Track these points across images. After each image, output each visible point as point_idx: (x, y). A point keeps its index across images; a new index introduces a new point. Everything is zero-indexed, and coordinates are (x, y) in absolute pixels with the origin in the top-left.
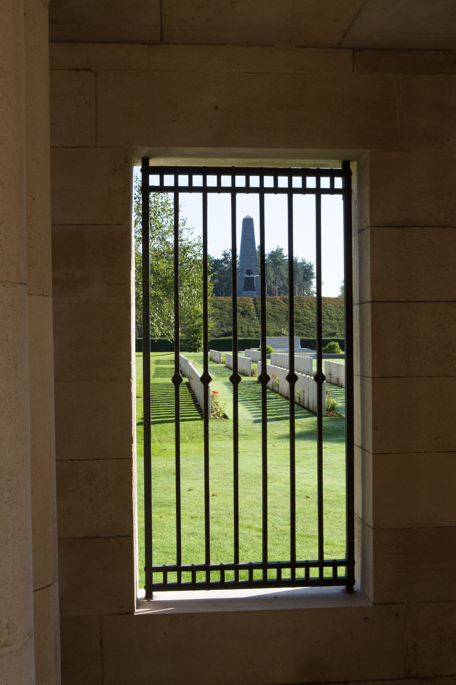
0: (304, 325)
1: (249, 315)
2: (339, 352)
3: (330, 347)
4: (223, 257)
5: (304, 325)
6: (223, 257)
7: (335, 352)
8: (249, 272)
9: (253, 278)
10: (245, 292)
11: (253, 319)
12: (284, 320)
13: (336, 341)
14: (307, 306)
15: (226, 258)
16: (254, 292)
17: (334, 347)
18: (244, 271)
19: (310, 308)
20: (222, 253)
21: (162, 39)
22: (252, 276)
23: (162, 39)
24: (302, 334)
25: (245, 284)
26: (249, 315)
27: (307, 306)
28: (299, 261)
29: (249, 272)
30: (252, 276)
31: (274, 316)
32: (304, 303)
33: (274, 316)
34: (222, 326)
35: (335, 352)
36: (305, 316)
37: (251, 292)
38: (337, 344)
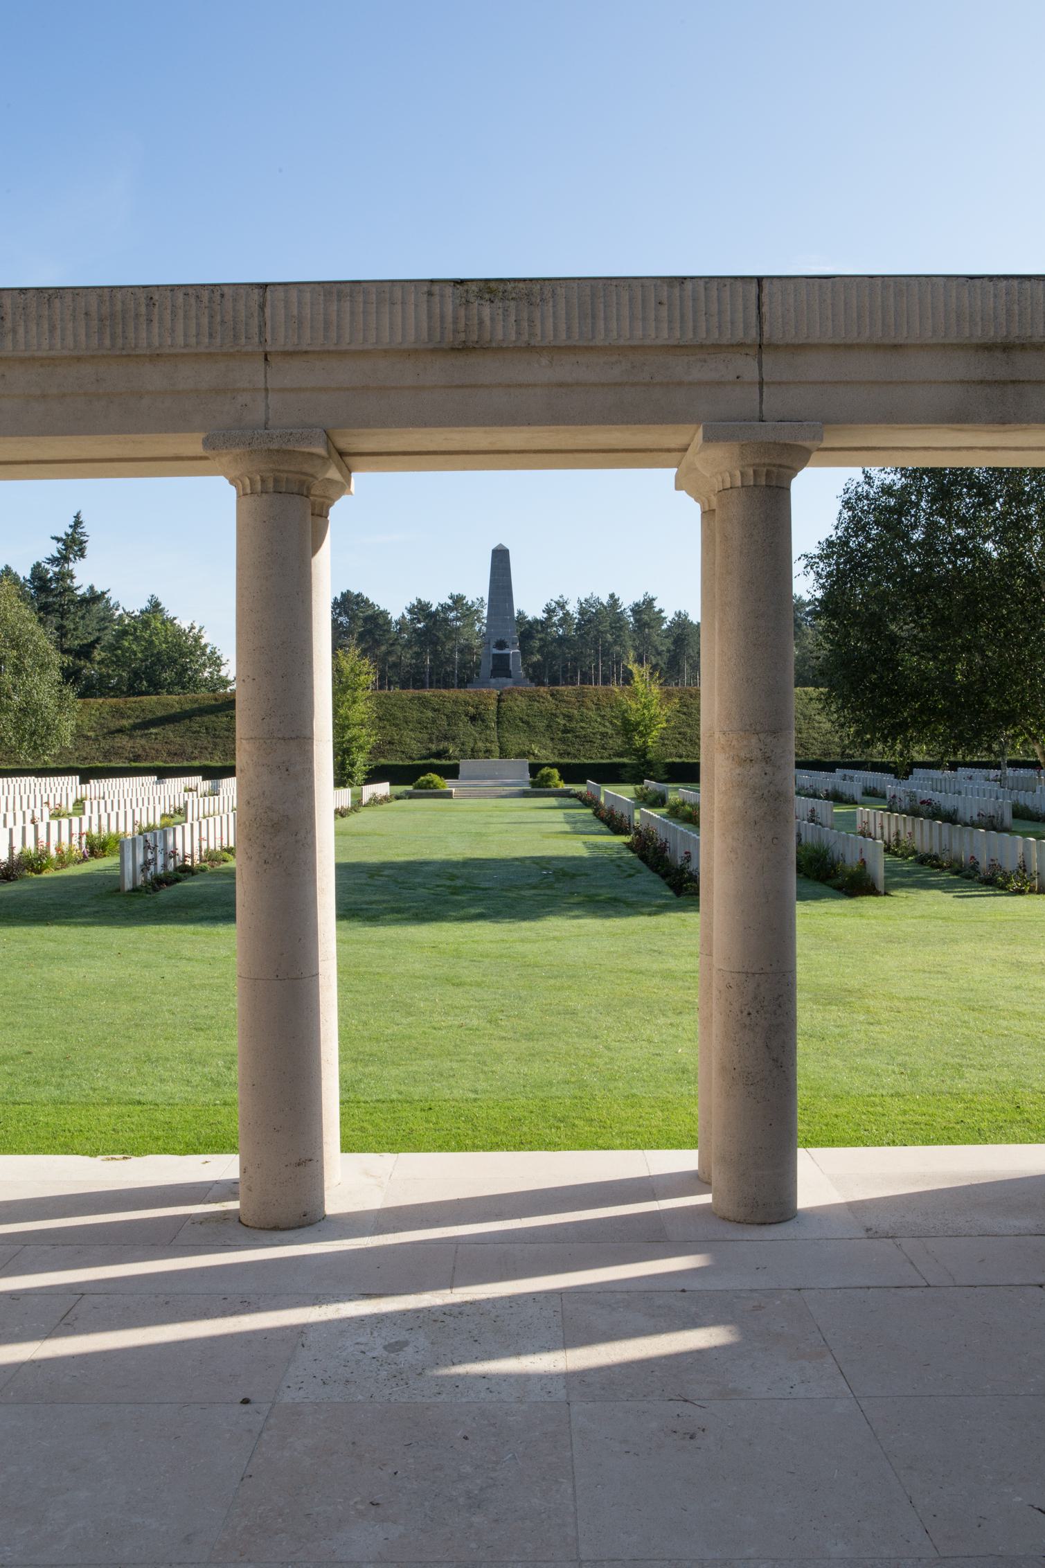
0: (577, 737)
1: (483, 721)
2: (556, 786)
3: (542, 777)
4: (545, 615)
5: (577, 737)
6: (545, 615)
7: (549, 786)
8: (501, 645)
9: (508, 655)
10: (493, 681)
11: (487, 727)
12: (542, 729)
13: (552, 766)
14: (590, 704)
15: (549, 618)
16: (510, 680)
17: (548, 777)
18: (493, 643)
19: (594, 707)
20: (543, 607)
21: (266, 423)
22: (505, 651)
23: (266, 423)
24: (569, 754)
25: (494, 666)
26: (483, 721)
27: (590, 704)
28: (669, 615)
29: (501, 645)
30: (505, 651)
31: (527, 723)
32: (586, 700)
33: (527, 723)
34: (431, 740)
35: (549, 786)
36: (582, 721)
37: (504, 680)
38: (555, 772)
